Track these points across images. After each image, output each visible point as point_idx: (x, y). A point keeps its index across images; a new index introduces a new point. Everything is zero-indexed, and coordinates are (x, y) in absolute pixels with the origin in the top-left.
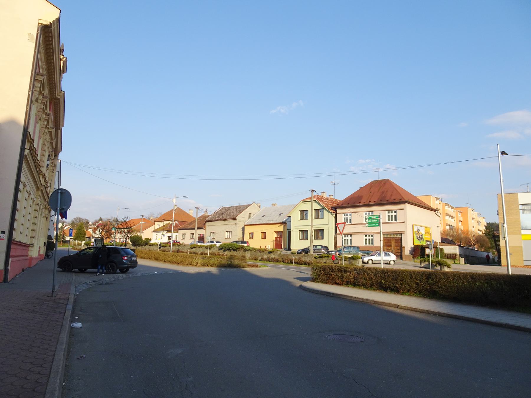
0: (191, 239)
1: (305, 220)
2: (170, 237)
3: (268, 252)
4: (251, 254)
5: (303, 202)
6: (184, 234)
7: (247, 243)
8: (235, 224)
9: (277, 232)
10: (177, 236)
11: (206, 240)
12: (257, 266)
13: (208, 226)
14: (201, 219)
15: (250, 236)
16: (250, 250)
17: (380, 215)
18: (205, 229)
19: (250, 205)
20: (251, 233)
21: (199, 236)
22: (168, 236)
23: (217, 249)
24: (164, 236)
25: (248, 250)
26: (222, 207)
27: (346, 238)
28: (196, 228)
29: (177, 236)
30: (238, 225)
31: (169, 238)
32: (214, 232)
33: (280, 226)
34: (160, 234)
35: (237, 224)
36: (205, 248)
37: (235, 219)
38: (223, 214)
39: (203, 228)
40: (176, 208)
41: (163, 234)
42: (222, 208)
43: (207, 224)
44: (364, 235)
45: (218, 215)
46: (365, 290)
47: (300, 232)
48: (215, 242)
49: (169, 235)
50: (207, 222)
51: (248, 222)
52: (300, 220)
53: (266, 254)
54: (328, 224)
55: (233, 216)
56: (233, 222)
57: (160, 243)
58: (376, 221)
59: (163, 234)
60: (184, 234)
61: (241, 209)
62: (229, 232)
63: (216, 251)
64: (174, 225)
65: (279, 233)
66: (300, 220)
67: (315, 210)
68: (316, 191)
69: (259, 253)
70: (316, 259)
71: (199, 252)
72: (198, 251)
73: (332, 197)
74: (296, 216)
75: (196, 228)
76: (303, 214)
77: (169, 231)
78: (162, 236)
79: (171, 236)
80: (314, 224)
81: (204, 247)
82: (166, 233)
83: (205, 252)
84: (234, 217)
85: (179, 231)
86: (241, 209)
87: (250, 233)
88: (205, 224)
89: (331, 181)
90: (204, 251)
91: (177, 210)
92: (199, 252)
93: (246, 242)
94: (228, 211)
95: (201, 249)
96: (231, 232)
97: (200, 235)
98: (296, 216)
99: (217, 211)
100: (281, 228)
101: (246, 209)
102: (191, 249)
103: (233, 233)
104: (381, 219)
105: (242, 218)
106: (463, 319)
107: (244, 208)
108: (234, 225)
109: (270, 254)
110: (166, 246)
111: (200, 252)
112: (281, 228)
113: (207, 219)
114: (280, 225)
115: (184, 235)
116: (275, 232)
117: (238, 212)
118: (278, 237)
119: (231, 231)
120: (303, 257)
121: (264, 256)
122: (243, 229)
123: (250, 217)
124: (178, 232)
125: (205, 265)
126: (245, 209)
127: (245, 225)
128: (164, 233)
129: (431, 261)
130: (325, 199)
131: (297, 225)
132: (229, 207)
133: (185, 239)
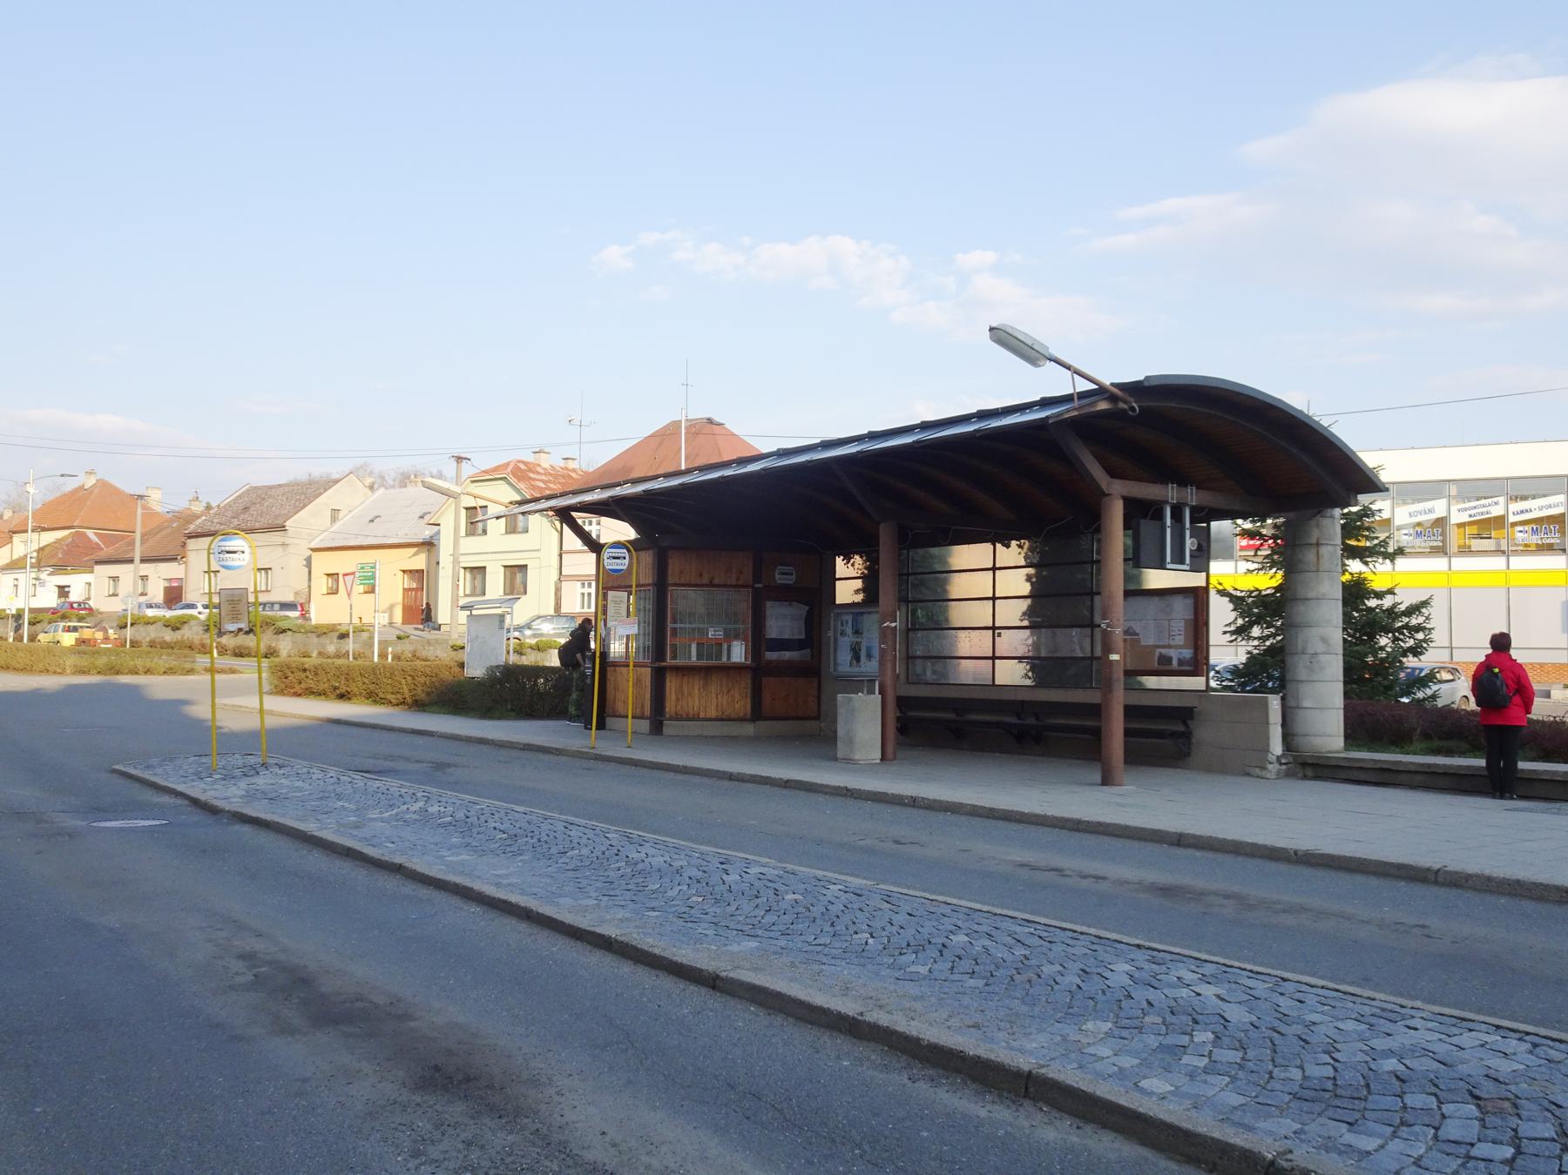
0: (110, 596)
1: (520, 532)
2: (67, 589)
3: (337, 634)
4: (294, 642)
5: (473, 482)
6: (115, 579)
7: (299, 609)
8: (283, 545)
9: (411, 571)
10: (89, 584)
11: (189, 597)
12: (233, 671)
13: (194, 553)
14: (174, 525)
15: (330, 585)
16: (289, 630)
17: (375, 563)
18: (185, 563)
19: (336, 481)
20: (332, 574)
21: (167, 584)
22: (59, 587)
23: (200, 629)
24: (43, 584)
25: (284, 631)
26: (247, 487)
27: (586, 590)
28: (137, 559)
29: (89, 584)
30: (290, 549)
31: (63, 591)
32: (266, 570)
33: (415, 554)
34: (25, 578)
35: (287, 545)
36: (165, 625)
37: (282, 528)
38: (246, 509)
39: (176, 559)
40: (95, 482)
41: (37, 579)
42: (248, 490)
43: (192, 544)
44: (579, 583)
45: (229, 514)
46: (419, 713)
47: (406, 576)
48: (199, 605)
49: (62, 580)
50: (190, 537)
51: (322, 540)
52: (507, 533)
53: (331, 643)
54: (538, 550)
55: (277, 517)
56: (275, 537)
57: (14, 612)
58: (370, 574)
59: (37, 579)
60: (115, 579)
61: (306, 492)
62: (263, 572)
63: (197, 634)
64: (34, 561)
65: (416, 574)
66: (507, 533)
67: (467, 509)
68: (469, 460)
69: (314, 639)
70: (455, 653)
71: (144, 638)
72: (144, 635)
73: (571, 465)
74: (450, 523)
75: (137, 559)
76: (475, 521)
77: (60, 568)
78: (35, 585)
79: (69, 586)
80: (461, 552)
81: (160, 624)
82: (49, 575)
83: (163, 637)
84: (279, 522)
85: (97, 568)
86: (306, 492)
87: (328, 575)
88: (185, 544)
89: (571, 416)
90: (161, 635)
91: (96, 491)
92: (144, 638)
93: (295, 605)
94: (264, 499)
95: (151, 628)
96: (270, 572)
97: (170, 580)
98: (450, 523)
99: (228, 501)
100: (419, 561)
101: (322, 496)
102: (121, 628)
103: (276, 574)
104: (377, 572)
105: (309, 524)
106: (615, 762)
107: (317, 492)
108: (280, 549)
109: (342, 641)
110: (38, 622)
111: (148, 639)
112: (419, 561)
113: (192, 527)
114: (415, 549)
115: (114, 581)
116: (404, 571)
117: (295, 504)
118: (415, 586)
119: (270, 569)
120: (423, 646)
121: (328, 647)
122: (309, 560)
123: (334, 519)
124: (92, 572)
125: (81, 671)
126: (321, 494)
127: (314, 550)
128: (43, 576)
129: (131, 643)
130: (542, 471)
131: (455, 549)
132: (270, 488)
133: (117, 595)
